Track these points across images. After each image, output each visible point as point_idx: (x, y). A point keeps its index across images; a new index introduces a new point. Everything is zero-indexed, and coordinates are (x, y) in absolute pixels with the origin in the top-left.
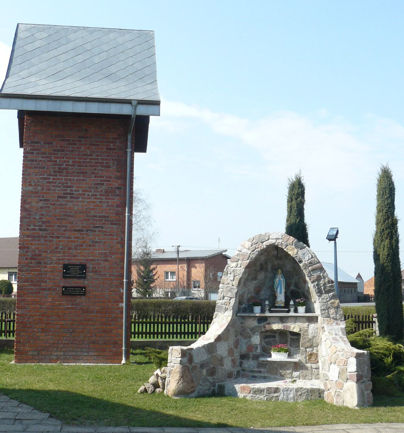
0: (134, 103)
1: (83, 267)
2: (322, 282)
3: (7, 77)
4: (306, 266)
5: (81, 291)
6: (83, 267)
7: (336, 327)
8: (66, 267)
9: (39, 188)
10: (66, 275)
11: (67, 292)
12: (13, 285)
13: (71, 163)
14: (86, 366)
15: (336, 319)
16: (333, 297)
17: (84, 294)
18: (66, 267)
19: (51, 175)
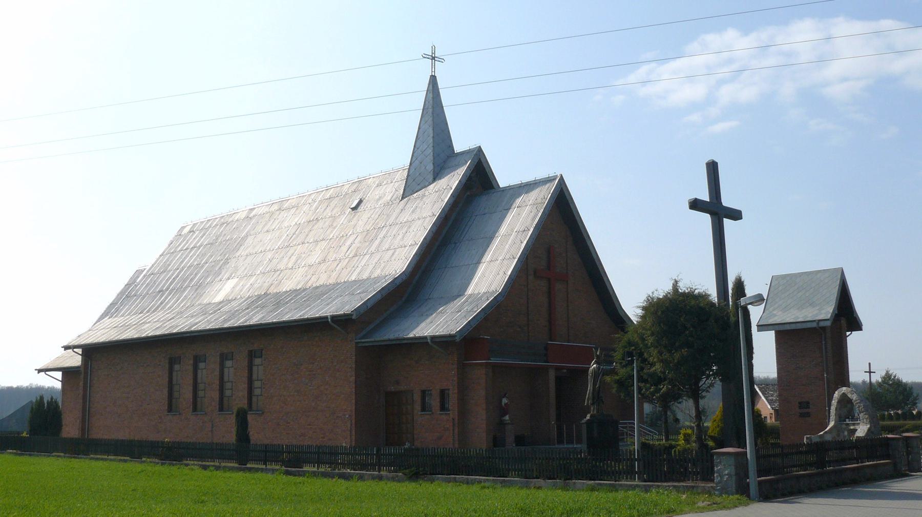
0: (817, 321)
1: (808, 403)
2: (860, 408)
3: (763, 312)
4: (855, 401)
5: (808, 415)
6: (808, 403)
7: (865, 426)
8: (800, 403)
9: (784, 366)
10: (800, 408)
11: (802, 415)
12: (61, 380)
13: (798, 352)
14: (632, 388)
15: (866, 423)
16: (865, 414)
17: (809, 416)
18: (800, 403)
19: (788, 359)
